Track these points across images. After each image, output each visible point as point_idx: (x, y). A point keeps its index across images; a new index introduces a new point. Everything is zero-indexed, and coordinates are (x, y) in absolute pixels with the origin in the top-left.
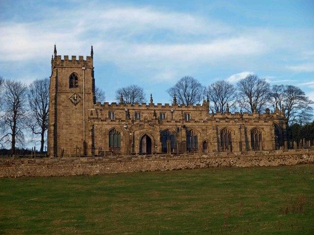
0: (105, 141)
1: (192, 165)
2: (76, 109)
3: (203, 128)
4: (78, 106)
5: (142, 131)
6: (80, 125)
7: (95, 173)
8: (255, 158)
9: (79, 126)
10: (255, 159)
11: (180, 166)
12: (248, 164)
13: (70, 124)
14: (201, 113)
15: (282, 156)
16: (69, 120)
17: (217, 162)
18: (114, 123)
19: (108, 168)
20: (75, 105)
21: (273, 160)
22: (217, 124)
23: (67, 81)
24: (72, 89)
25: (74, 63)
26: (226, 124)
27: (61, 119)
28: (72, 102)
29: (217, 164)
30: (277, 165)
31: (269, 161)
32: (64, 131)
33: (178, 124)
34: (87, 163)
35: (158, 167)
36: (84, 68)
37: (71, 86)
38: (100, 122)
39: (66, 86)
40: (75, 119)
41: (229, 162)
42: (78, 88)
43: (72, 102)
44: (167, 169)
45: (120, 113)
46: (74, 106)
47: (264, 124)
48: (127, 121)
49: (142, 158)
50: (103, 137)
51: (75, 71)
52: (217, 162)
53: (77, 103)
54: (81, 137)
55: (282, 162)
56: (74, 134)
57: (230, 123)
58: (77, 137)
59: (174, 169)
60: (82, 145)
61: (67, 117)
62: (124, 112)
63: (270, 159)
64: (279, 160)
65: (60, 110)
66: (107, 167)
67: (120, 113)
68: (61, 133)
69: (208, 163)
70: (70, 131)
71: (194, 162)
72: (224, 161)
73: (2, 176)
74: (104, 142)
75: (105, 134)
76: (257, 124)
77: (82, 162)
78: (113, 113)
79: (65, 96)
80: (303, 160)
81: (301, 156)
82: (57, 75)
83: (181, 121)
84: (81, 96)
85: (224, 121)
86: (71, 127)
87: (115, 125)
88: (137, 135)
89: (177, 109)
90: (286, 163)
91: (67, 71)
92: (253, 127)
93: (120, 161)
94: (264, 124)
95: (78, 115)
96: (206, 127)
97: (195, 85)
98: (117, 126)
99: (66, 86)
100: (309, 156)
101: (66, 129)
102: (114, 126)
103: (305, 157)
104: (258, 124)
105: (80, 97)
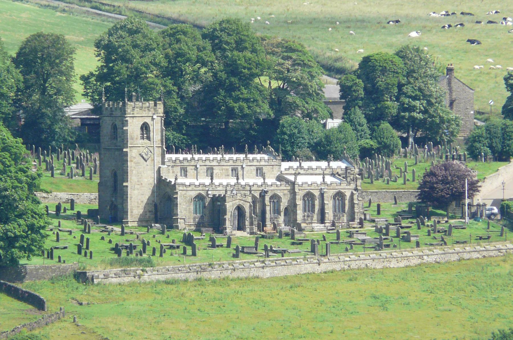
0: (189, 209)
1: (337, 267)
5: (234, 202)
13: (141, 184)
18: (198, 189)
19: (276, 272)
26: (309, 188)
30: (403, 266)
31: (398, 262)
32: (136, 192)
38: (185, 188)
39: (137, 139)
47: (347, 187)
61: (138, 176)
71: (339, 265)
74: (188, 210)
76: (339, 187)
79: (136, 150)
86: (142, 187)
92: (337, 191)
94: (347, 187)
99: (137, 139)
101: (138, 189)
102: (199, 192)
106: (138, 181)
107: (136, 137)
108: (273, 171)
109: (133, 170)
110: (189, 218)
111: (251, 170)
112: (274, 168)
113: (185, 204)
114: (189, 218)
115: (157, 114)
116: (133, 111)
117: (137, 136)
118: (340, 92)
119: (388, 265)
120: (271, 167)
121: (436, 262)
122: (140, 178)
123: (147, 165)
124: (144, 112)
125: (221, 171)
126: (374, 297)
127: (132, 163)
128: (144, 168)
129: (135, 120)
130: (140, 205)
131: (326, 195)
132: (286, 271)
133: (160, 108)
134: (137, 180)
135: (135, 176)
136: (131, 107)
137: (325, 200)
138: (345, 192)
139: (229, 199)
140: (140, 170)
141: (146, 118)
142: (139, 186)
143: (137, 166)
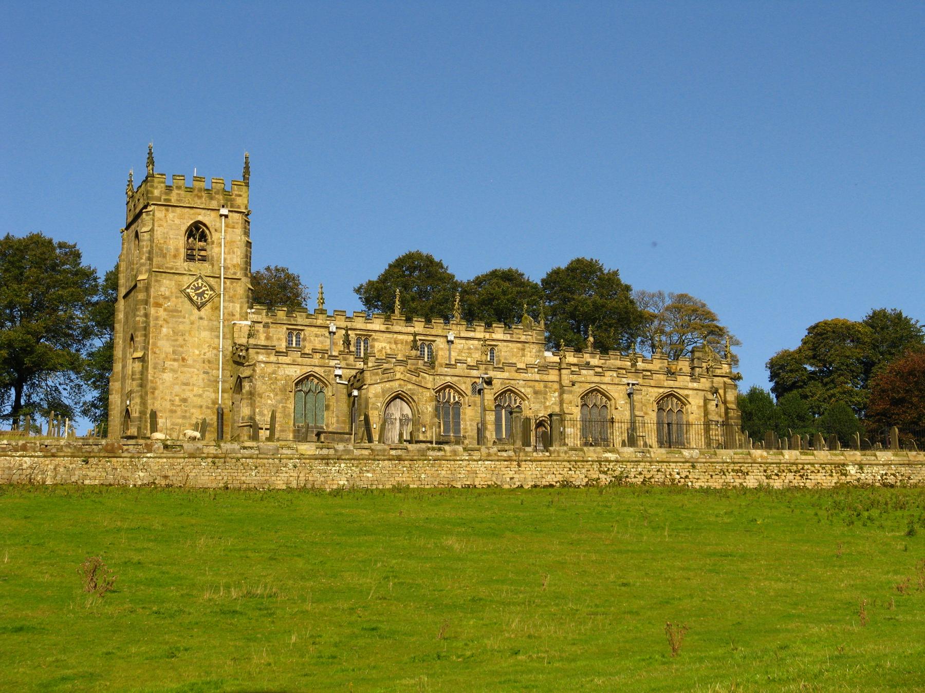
1: (579, 478)
2: (201, 318)
3: (537, 389)
4: (204, 312)
5: (388, 385)
6: (209, 362)
7: (335, 487)
8: (731, 467)
9: (206, 366)
10: (733, 470)
11: (550, 479)
12: (716, 483)
13: (183, 359)
14: (523, 350)
15: (796, 464)
16: (182, 346)
17: (640, 474)
18: (307, 361)
19: (370, 475)
20: (199, 309)
21: (777, 475)
22: (574, 378)
23: (178, 242)
24: (194, 267)
25: (200, 197)
26: (597, 379)
27: (160, 343)
28: (191, 300)
29: (640, 479)
32: (167, 376)
33: (475, 373)
34: (315, 458)
35: (494, 479)
36: (224, 211)
37: (190, 258)
38: (273, 358)
39: (175, 256)
40: (199, 346)
41: (670, 475)
42: (206, 264)
43: (191, 300)
44: (519, 483)
45: (317, 336)
46: (196, 311)
47: (691, 385)
48: (345, 359)
49: (455, 453)
50: (279, 398)
51: (200, 218)
52: (640, 474)
53: (204, 304)
54: (213, 396)
55: (797, 481)
56: (194, 385)
57: (607, 379)
58: (200, 396)
59: (535, 486)
60: (215, 417)
61: (176, 340)
62: (327, 334)
63: (769, 472)
64: (790, 476)
65: (157, 318)
66: (368, 471)
67: (317, 336)
68: (159, 382)
69: (617, 473)
70: (183, 378)
71: (584, 471)
72: (658, 471)
73: (97, 482)
75: (283, 390)
76: (671, 383)
77: (302, 457)
78: (298, 336)
80: (849, 479)
81: (841, 468)
82: (153, 225)
83: (482, 367)
84: (216, 287)
85: (591, 372)
86: (183, 366)
87: (314, 365)
88: (376, 396)
89: (462, 335)
90: (809, 484)
91: (181, 217)
92: (666, 390)
93: (399, 459)
94: (691, 385)
95: (205, 334)
96: (545, 387)
97: (454, 276)
98: (317, 369)
99: (175, 256)
100: (861, 468)
101: (174, 371)
102: (309, 369)
103: (852, 470)
104: (676, 384)
105: (212, 289)
106: (174, 352)
107: (172, 252)
108: (523, 355)
109: (161, 326)
110: (282, 431)
111: (469, 349)
112: (527, 349)
113: (272, 395)
114: (282, 431)
115: (231, 207)
116: (166, 194)
117: (177, 250)
118: (770, 381)
119: (738, 481)
120: (519, 345)
121: (885, 485)
122: (182, 346)
123: (201, 318)
124: (199, 201)
125: (394, 346)
126: (782, 648)
127: (161, 310)
128: (192, 323)
129: (172, 215)
130: (179, 409)
131: (639, 397)
132: (406, 475)
133: (240, 196)
134: (171, 350)
135: (168, 340)
136: (162, 185)
137: (636, 409)
138: (687, 396)
139: (374, 378)
140: (181, 327)
141: (204, 211)
142: (176, 364)
143: (174, 317)
